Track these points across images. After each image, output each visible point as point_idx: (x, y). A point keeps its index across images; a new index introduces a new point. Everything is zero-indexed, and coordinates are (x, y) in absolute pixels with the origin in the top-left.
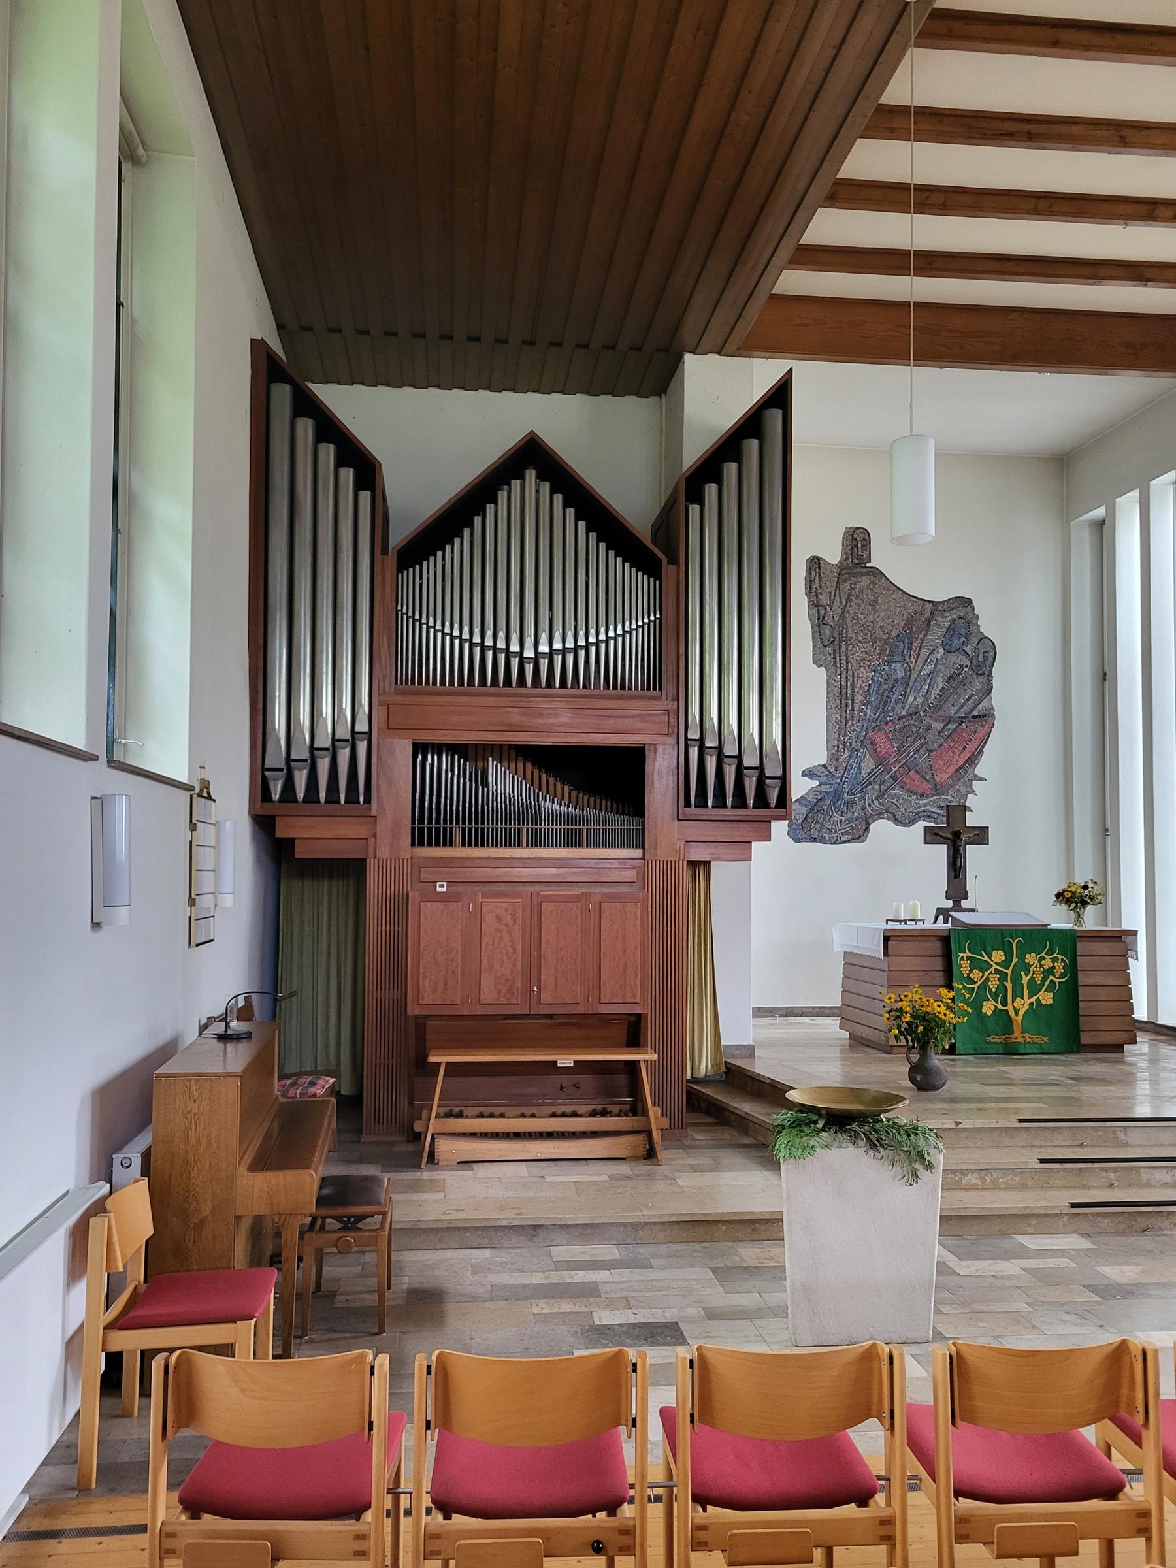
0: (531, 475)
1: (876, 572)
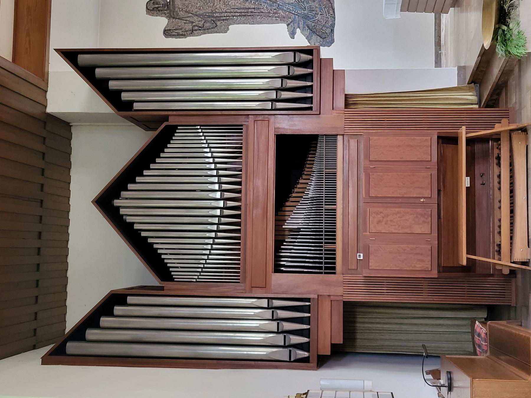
0: (117, 203)
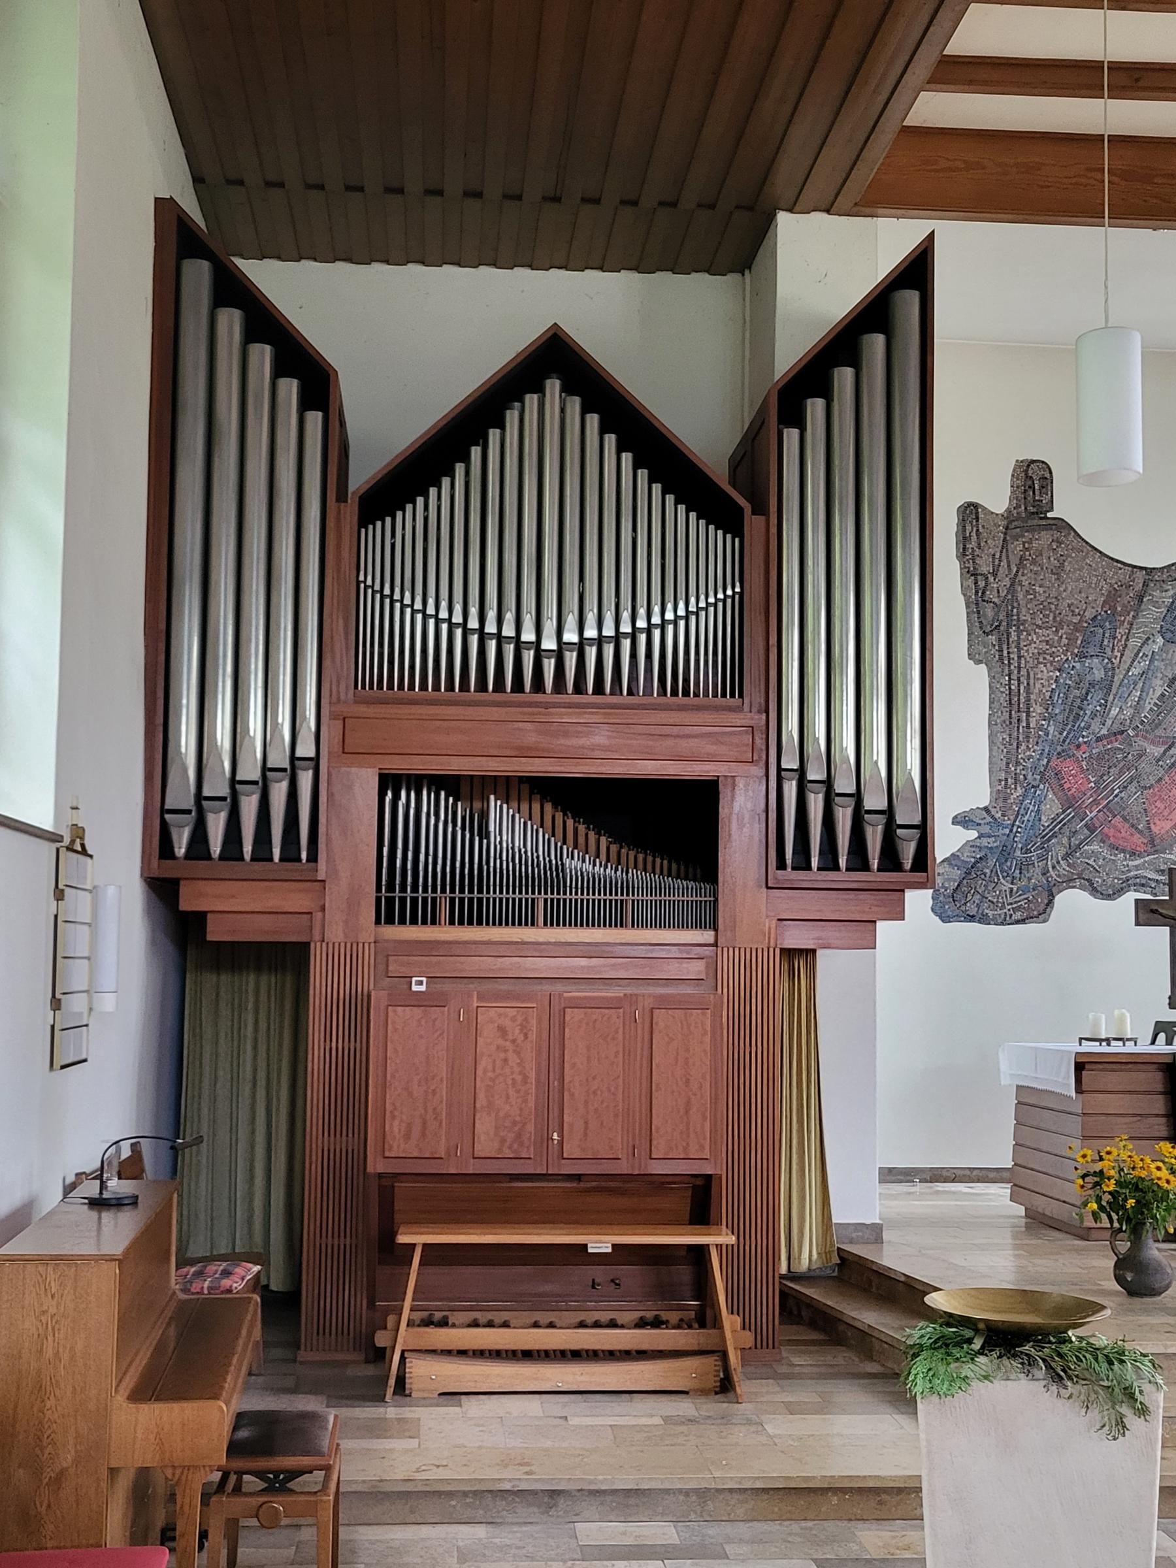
0: (553, 386)
1: (1062, 526)
